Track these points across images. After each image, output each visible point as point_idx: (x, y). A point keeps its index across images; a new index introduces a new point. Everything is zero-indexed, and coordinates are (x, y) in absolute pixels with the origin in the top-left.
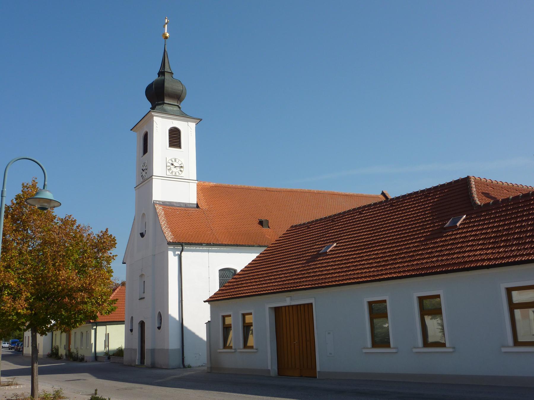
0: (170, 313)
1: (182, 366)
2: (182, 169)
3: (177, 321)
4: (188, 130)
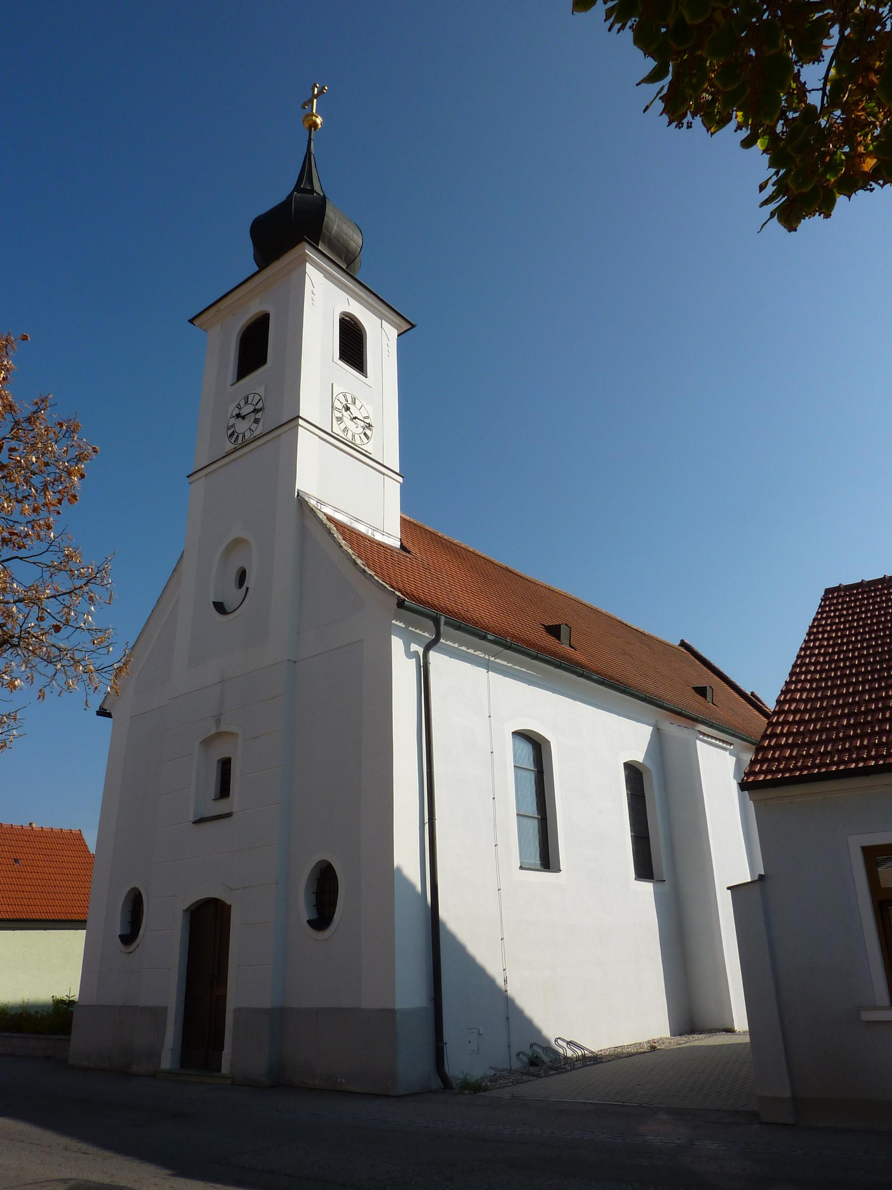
0: (397, 861)
1: (437, 1083)
2: (368, 432)
3: (417, 893)
4: (382, 339)
